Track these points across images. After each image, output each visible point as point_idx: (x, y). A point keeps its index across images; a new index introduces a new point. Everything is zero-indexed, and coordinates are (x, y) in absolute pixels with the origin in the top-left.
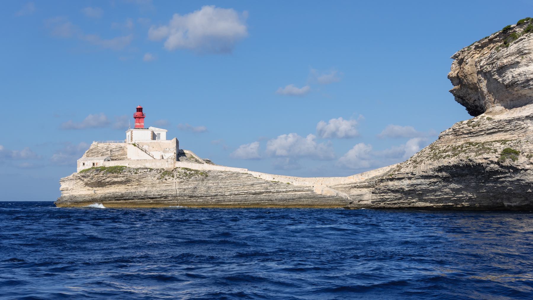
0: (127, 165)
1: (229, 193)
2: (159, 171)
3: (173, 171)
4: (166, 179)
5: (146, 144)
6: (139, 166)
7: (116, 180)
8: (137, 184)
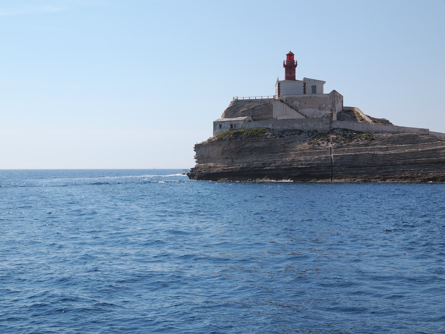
0: (270, 126)
1: (402, 161)
2: (310, 134)
3: (328, 133)
4: (319, 144)
5: (297, 99)
6: (286, 127)
7: (256, 145)
8: (283, 150)
